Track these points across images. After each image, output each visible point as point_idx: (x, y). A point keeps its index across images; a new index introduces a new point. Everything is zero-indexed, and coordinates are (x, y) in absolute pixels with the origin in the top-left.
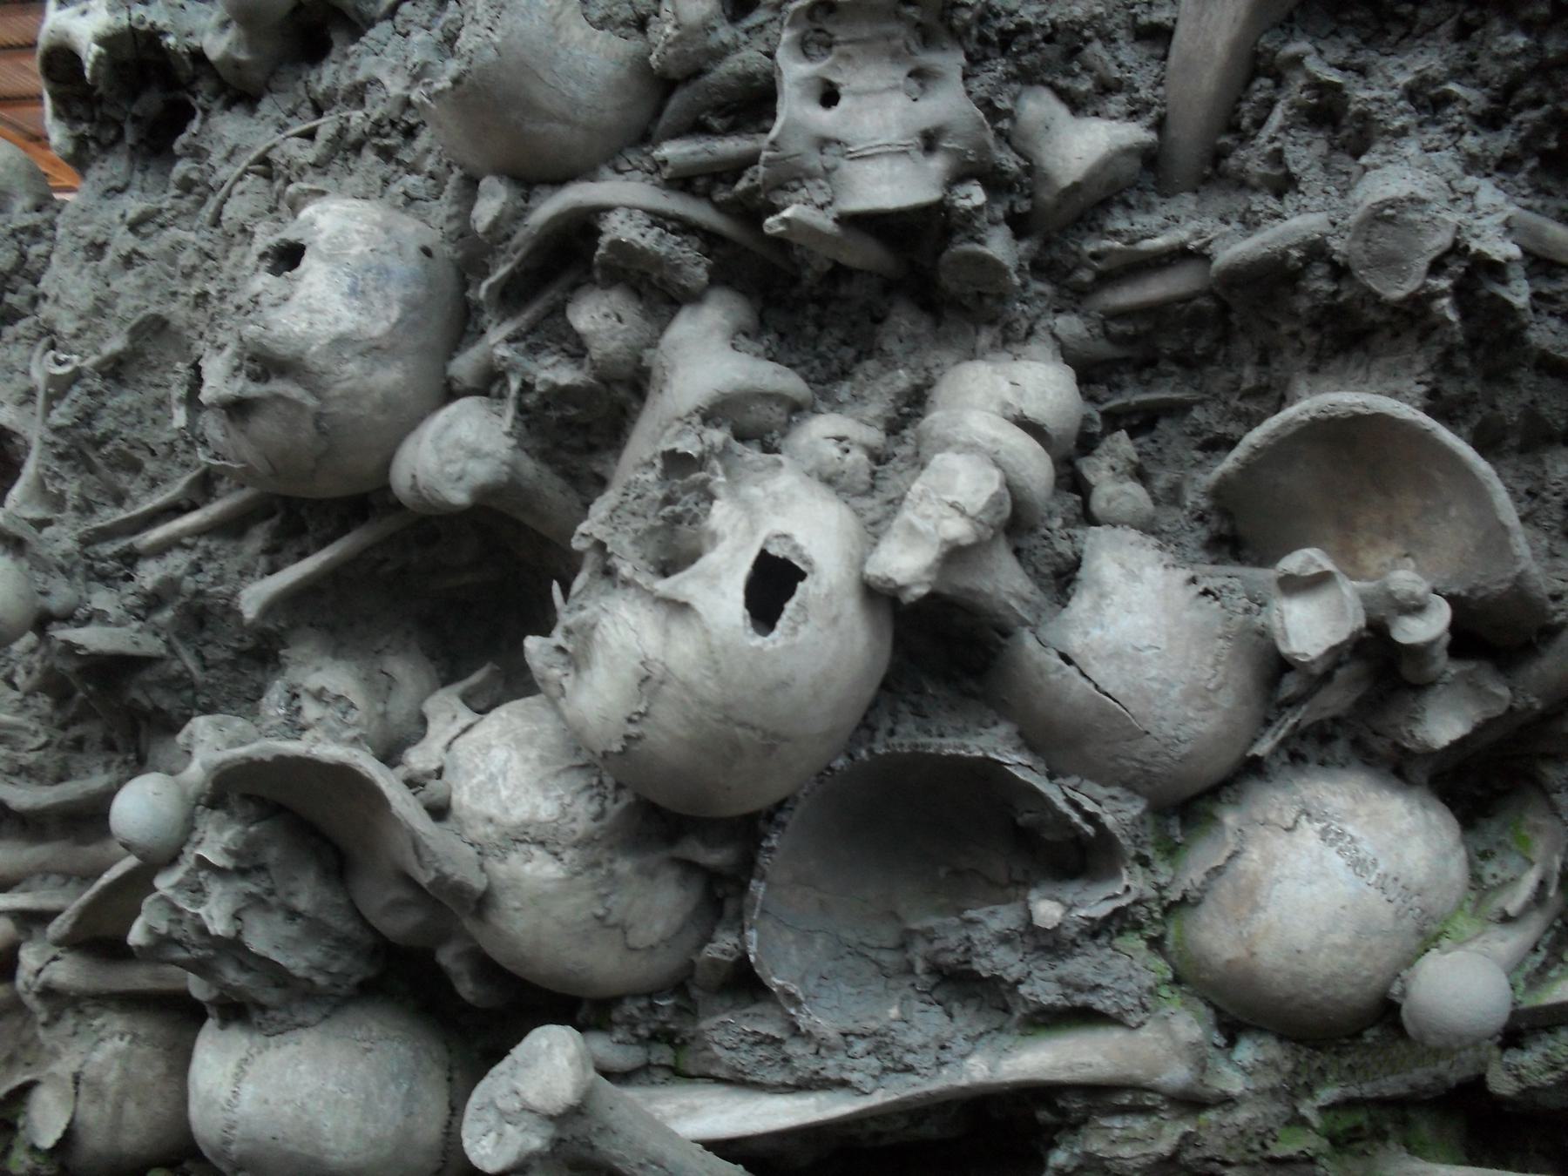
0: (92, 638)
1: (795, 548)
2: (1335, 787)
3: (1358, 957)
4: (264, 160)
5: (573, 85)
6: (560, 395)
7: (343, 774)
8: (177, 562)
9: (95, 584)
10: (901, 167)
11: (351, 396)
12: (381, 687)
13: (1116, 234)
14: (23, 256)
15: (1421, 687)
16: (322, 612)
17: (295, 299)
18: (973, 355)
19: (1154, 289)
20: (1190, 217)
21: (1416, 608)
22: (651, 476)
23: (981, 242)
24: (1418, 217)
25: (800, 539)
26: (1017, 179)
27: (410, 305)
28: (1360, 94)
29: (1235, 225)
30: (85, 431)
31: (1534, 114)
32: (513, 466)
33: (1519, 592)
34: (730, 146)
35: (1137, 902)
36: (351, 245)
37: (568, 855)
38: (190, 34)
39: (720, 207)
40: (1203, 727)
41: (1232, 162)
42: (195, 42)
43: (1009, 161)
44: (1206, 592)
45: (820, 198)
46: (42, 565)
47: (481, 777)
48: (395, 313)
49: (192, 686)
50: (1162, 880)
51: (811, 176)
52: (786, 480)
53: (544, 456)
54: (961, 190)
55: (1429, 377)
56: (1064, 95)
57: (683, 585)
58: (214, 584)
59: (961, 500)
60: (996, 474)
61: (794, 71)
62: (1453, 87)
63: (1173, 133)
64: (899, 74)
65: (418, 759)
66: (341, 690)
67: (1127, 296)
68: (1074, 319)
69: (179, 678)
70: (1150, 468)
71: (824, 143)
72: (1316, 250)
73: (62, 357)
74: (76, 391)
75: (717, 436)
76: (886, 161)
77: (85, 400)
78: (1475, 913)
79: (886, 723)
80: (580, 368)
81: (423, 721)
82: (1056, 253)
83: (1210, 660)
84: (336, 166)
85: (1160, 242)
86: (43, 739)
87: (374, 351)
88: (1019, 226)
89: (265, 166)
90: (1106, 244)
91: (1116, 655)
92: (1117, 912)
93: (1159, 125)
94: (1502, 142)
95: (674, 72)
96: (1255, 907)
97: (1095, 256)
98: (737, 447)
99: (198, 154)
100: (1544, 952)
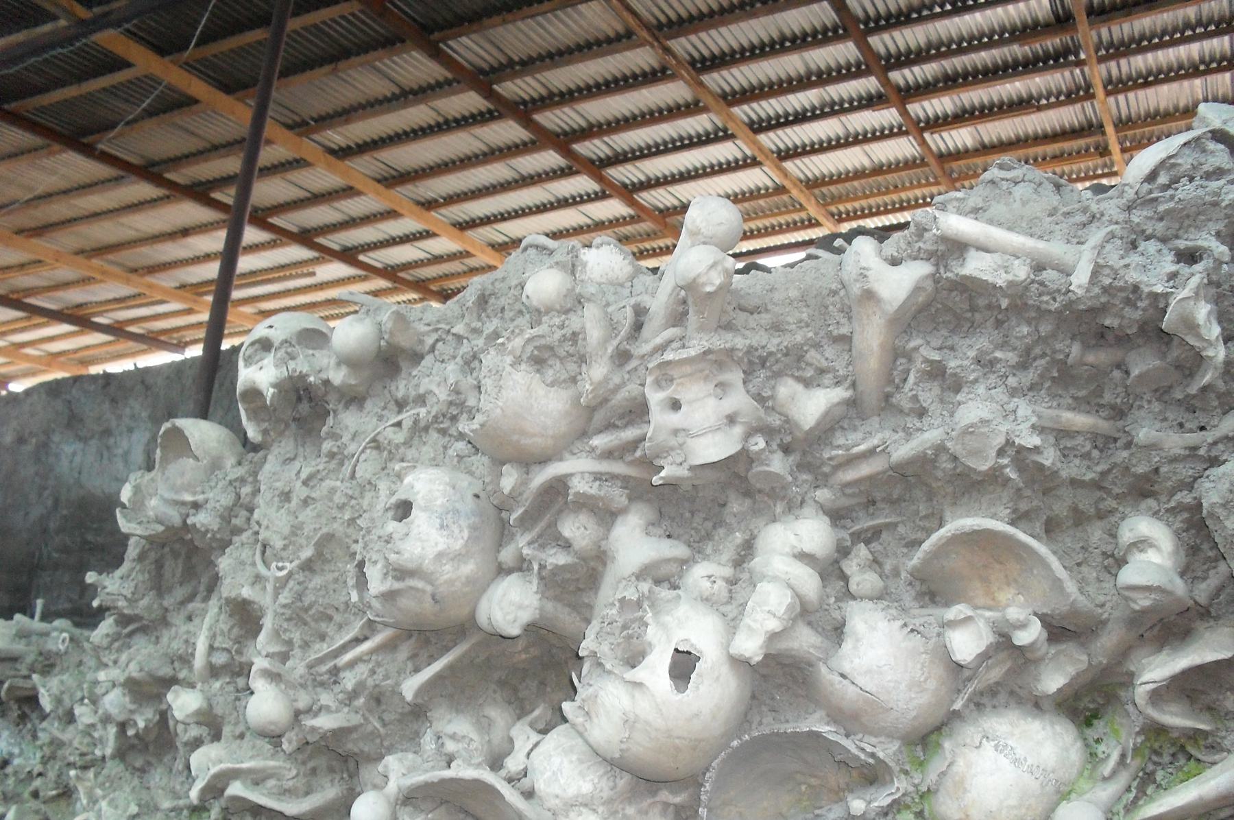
0: (325, 722)
1: (692, 645)
2: (1001, 720)
3: (1024, 811)
4: (374, 440)
5: (543, 418)
6: (558, 569)
7: (478, 784)
8: (362, 670)
9: (319, 689)
10: (719, 437)
11: (451, 582)
12: (485, 726)
13: (839, 447)
14: (238, 496)
15: (1037, 662)
16: (454, 689)
17: (412, 535)
18: (774, 520)
19: (865, 469)
20: (877, 431)
21: (1023, 626)
22: (614, 611)
23: (767, 465)
24: (986, 429)
25: (694, 641)
26: (781, 427)
27: (473, 528)
28: (952, 364)
29: (901, 434)
30: (299, 604)
31: (1043, 362)
32: (541, 609)
33: (1074, 612)
34: (630, 434)
35: (904, 795)
36: (436, 499)
37: (600, 809)
38: (320, 371)
39: (631, 463)
40: (921, 701)
41: (894, 400)
42: (324, 376)
43: (775, 420)
44: (912, 630)
45: (679, 460)
46: (291, 686)
47: (548, 774)
48: (466, 534)
49: (380, 736)
50: (916, 782)
51: (672, 449)
52: (684, 610)
53: (557, 598)
54: (752, 441)
55: (1010, 505)
56: (799, 379)
57: (639, 674)
58: (384, 680)
59: (773, 609)
60: (789, 593)
61: (655, 398)
62: (998, 354)
63: (860, 388)
64: (710, 387)
65: (513, 764)
66: (465, 733)
67: (850, 475)
68: (826, 490)
69: (372, 733)
70: (880, 559)
71: (676, 432)
72: (940, 448)
73: (280, 564)
74: (291, 583)
75: (645, 587)
76: (710, 435)
77: (297, 587)
78: (1090, 777)
79: (757, 719)
80: (569, 553)
81: (511, 741)
82: (809, 458)
83: (919, 666)
84: (416, 441)
85: (862, 447)
86: (294, 772)
87: (459, 557)
88: (786, 450)
89: (376, 444)
90: (834, 453)
91: (869, 671)
92: (894, 801)
93: (854, 385)
94: (1029, 377)
95: (593, 403)
96: (965, 791)
97: (830, 459)
98: (657, 589)
99: (335, 436)
100: (1134, 791)
